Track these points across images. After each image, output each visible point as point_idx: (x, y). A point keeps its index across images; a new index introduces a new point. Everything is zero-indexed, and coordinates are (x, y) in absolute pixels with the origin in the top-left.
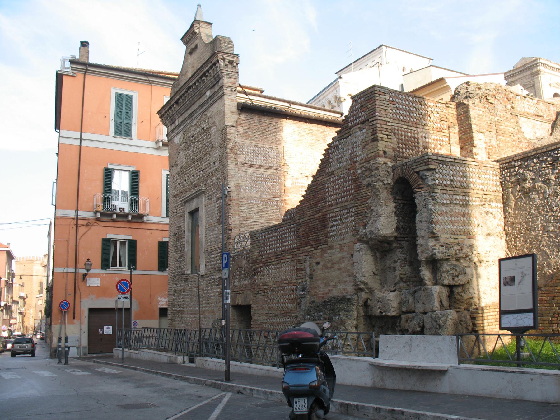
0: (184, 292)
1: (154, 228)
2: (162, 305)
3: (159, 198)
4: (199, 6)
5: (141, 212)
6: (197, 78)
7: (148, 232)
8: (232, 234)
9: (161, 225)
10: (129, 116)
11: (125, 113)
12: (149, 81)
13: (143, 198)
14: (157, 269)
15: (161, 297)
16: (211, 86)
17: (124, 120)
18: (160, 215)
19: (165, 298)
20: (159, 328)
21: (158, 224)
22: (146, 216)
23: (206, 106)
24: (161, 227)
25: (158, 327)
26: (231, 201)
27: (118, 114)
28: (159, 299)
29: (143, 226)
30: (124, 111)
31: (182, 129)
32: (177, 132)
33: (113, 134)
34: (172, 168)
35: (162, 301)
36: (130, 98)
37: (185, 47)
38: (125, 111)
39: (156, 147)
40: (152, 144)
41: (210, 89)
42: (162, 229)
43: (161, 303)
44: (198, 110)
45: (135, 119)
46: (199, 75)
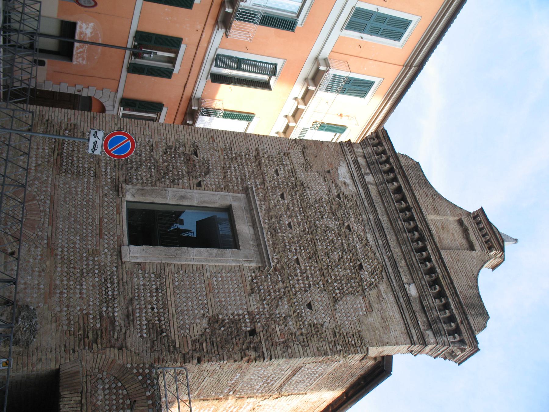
0: (95, 175)
1: (204, 36)
2: (81, 27)
3: (247, 50)
4: (516, 240)
5: (236, 24)
6: (438, 270)
7: (200, 27)
8: (190, 365)
9: (206, 45)
10: (374, 32)
11: (380, 27)
12: (411, 67)
13: (253, 28)
14: (139, 29)
15: (94, 28)
16: (424, 303)
17: (372, 23)
18: (220, 46)
19: (91, 33)
20: (39, 16)
21: (209, 42)
22: (226, 33)
23: (394, 281)
24: (203, 44)
25: (43, 13)
26: (248, 361)
27: (382, 18)
28: (91, 25)
29: (211, 21)
30: (383, 26)
31: (359, 194)
32: (355, 174)
33: (358, 6)
34: (300, 148)
35: (87, 28)
36: (397, 37)
37: (472, 212)
38: (383, 27)
39: (320, 57)
40: (326, 53)
41: (420, 297)
42: (200, 45)
43: (84, 26)
44: (388, 254)
45: (367, 37)
46: (443, 278)
